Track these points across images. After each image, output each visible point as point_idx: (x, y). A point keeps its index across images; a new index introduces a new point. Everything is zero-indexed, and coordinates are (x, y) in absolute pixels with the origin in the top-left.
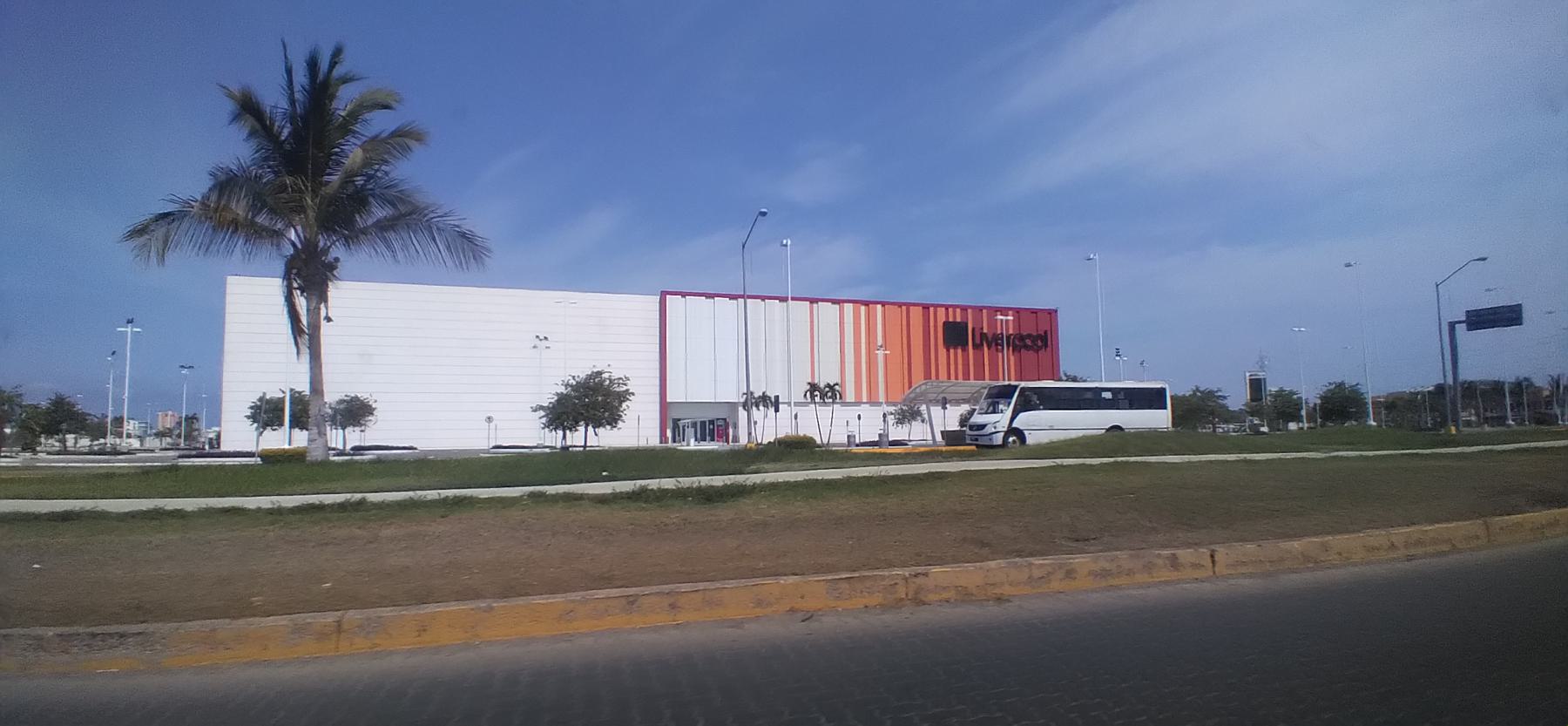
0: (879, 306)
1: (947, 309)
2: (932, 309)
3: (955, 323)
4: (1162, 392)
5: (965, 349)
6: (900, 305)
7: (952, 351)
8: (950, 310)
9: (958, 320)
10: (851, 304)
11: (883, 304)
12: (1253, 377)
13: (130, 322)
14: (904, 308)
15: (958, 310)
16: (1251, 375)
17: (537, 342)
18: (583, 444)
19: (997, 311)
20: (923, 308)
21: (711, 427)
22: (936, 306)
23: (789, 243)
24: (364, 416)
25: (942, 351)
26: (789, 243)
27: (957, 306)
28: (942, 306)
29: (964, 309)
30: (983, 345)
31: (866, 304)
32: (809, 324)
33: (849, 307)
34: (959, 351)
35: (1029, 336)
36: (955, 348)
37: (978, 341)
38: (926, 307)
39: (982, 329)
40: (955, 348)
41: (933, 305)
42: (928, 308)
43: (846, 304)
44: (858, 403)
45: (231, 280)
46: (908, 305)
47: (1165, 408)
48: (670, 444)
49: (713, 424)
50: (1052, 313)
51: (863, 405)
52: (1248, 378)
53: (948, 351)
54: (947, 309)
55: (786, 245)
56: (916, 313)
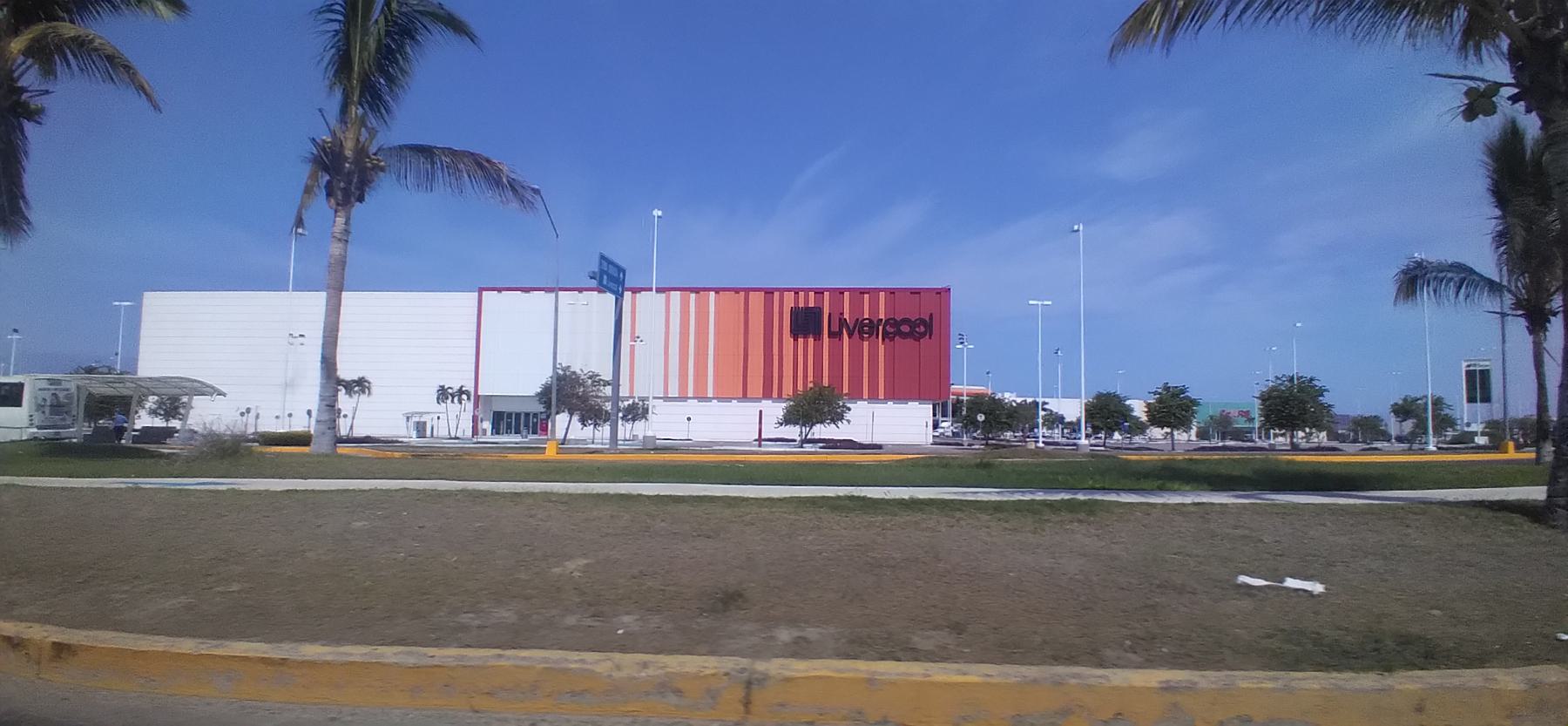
0: (712, 294)
1: (796, 293)
2: (777, 294)
3: (807, 308)
4: (19, 387)
5: (818, 336)
6: (737, 291)
7: (801, 340)
8: (802, 294)
9: (812, 304)
10: (679, 292)
11: (717, 291)
12: (1471, 368)
13: (16, 331)
14: (742, 293)
15: (812, 294)
16: (1469, 366)
17: (291, 340)
18: (757, 437)
19: (864, 293)
20: (766, 293)
21: (535, 420)
22: (782, 291)
23: (1081, 228)
24: (1402, 407)
25: (788, 341)
26: (1081, 228)
27: (811, 290)
28: (789, 290)
29: (819, 292)
30: (842, 333)
31: (697, 291)
32: (637, 310)
33: (676, 296)
34: (811, 340)
35: (905, 321)
36: (805, 337)
37: (835, 328)
38: (769, 292)
39: (842, 314)
40: (805, 337)
41: (777, 290)
42: (773, 293)
43: (672, 292)
44: (683, 398)
45: (324, 294)
46: (747, 290)
47: (19, 405)
48: (489, 438)
49: (537, 419)
50: (943, 293)
51: (689, 401)
52: (1464, 370)
53: (796, 340)
54: (796, 293)
55: (1078, 231)
56: (757, 300)
